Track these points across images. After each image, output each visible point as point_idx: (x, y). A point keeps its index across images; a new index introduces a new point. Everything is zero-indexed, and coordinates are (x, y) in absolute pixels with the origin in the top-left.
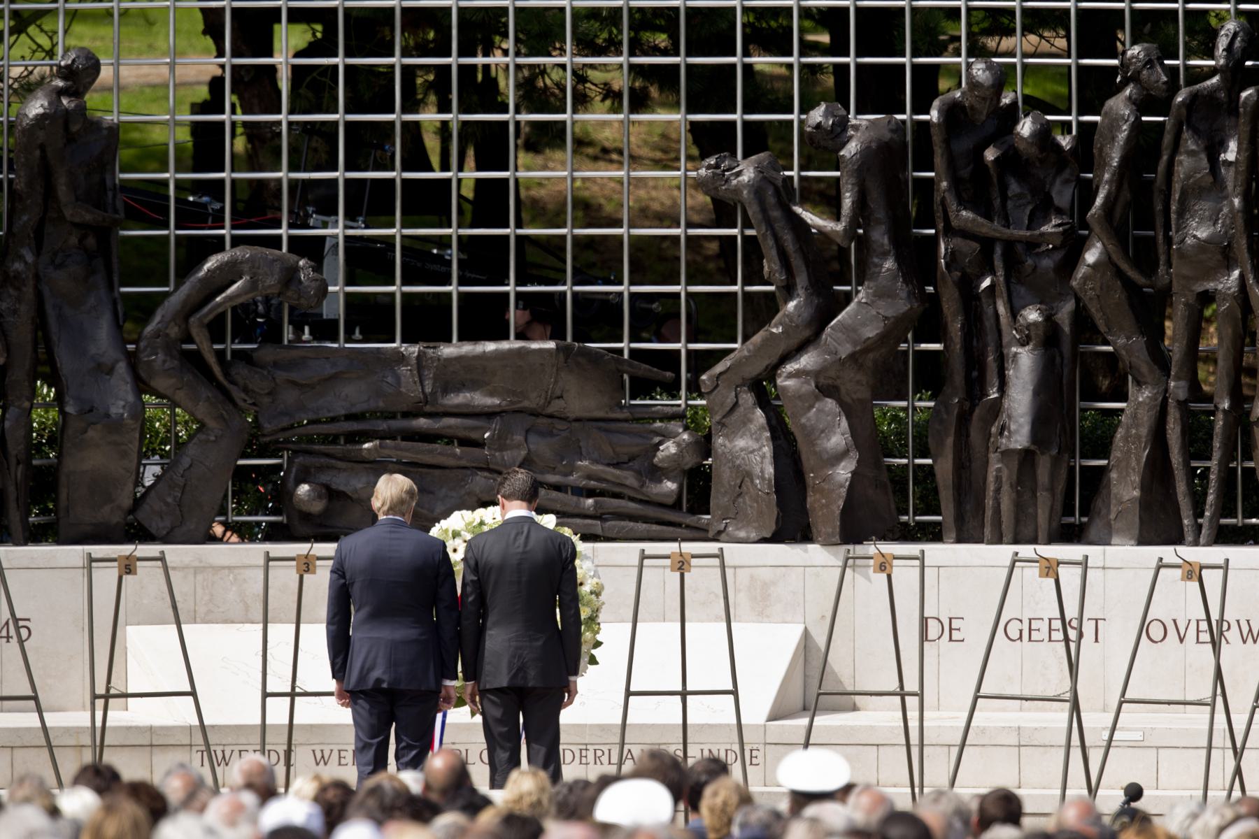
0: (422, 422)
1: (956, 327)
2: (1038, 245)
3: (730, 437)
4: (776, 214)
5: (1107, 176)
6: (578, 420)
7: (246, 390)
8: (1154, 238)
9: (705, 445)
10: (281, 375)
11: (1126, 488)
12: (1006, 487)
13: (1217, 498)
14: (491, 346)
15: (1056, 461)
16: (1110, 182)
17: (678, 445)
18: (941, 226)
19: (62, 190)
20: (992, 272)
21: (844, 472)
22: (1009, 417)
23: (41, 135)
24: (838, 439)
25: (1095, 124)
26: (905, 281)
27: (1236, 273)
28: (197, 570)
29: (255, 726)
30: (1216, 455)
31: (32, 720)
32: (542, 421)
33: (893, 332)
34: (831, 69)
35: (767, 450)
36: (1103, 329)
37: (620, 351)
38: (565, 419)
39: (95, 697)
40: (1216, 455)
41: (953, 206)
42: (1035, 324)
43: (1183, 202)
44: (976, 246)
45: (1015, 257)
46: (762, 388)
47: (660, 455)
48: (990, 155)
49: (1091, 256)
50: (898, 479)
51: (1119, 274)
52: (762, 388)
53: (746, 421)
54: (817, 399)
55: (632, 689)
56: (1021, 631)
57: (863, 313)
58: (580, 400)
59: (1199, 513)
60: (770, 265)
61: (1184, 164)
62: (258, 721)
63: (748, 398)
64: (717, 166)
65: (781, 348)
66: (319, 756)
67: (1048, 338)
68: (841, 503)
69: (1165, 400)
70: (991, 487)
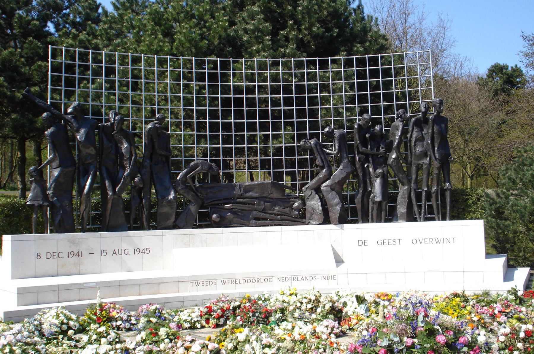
0: (241, 200)
7: (201, 193)
9: (304, 203)
10: (209, 191)
11: (402, 209)
19: (156, 146)
20: (369, 162)
21: (338, 208)
24: (337, 200)
27: (428, 159)
32: (268, 199)
34: (77, 230)
35: (320, 204)
38: (272, 199)
41: (360, 147)
42: (381, 173)
46: (317, 190)
48: (367, 136)
52: (317, 190)
56: (382, 243)
57: (338, 173)
59: (420, 214)
60: (318, 162)
61: (415, 135)
63: (314, 192)
65: (322, 180)
67: (384, 177)
70: (370, 210)
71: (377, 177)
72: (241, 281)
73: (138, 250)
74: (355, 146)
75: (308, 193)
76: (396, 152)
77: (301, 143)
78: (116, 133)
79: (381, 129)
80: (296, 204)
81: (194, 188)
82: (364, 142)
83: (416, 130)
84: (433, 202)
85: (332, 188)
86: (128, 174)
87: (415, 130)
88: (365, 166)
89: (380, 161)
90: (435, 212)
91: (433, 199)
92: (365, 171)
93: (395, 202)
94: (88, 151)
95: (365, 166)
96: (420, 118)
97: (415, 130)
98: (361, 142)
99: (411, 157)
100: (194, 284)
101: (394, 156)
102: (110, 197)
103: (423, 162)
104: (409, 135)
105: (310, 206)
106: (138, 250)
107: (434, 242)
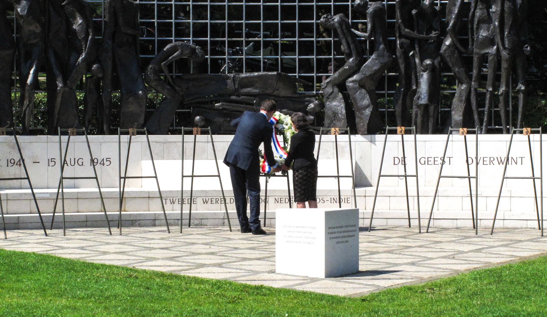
2: (428, 41)
4: (345, 31)
5: (454, 17)
6: (283, 97)
8: (468, 39)
9: (322, 105)
11: (457, 116)
12: (419, 116)
13: (487, 119)
14: (256, 74)
15: (435, 108)
16: (455, 18)
17: (314, 104)
18: (397, 35)
19: (121, 20)
20: (414, 49)
21: (368, 112)
22: (421, 94)
24: (366, 101)
25: (446, 3)
26: (387, 52)
27: (495, 47)
28: (164, 143)
29: (188, 191)
31: (30, 191)
33: (383, 67)
35: (343, 105)
36: (451, 65)
37: (296, 76)
39: (121, 178)
41: (403, 27)
42: (429, 64)
43: (478, 24)
44: (408, 41)
45: (423, 43)
46: (342, 87)
47: (308, 108)
48: (414, 12)
49: (448, 43)
50: (382, 114)
51: (457, 48)
52: (342, 87)
54: (359, 89)
55: (382, 174)
57: (372, 63)
60: (343, 48)
61: (478, 13)
62: (180, 189)
63: (336, 90)
64: (326, 17)
66: (205, 201)
67: (433, 71)
68: (367, 121)
69: (470, 88)
71: (424, 71)
73: (12, 161)
74: (397, 26)
75: (329, 90)
76: (451, 37)
77: (322, 19)
78: (66, 4)
80: (312, 105)
81: (170, 80)
83: (481, 6)
84: (501, 108)
85: (361, 84)
86: (83, 60)
87: (480, 6)
88: (411, 54)
89: (431, 49)
90: (503, 122)
91: (501, 105)
92: (409, 62)
93: (450, 106)
94: (32, 28)
95: (411, 54)
97: (480, 6)
98: (403, 22)
99: (473, 45)
100: (168, 201)
101: (448, 43)
102: (60, 90)
103: (487, 51)
104: (470, 14)
105: (331, 108)
106: (12, 161)
107: (496, 162)
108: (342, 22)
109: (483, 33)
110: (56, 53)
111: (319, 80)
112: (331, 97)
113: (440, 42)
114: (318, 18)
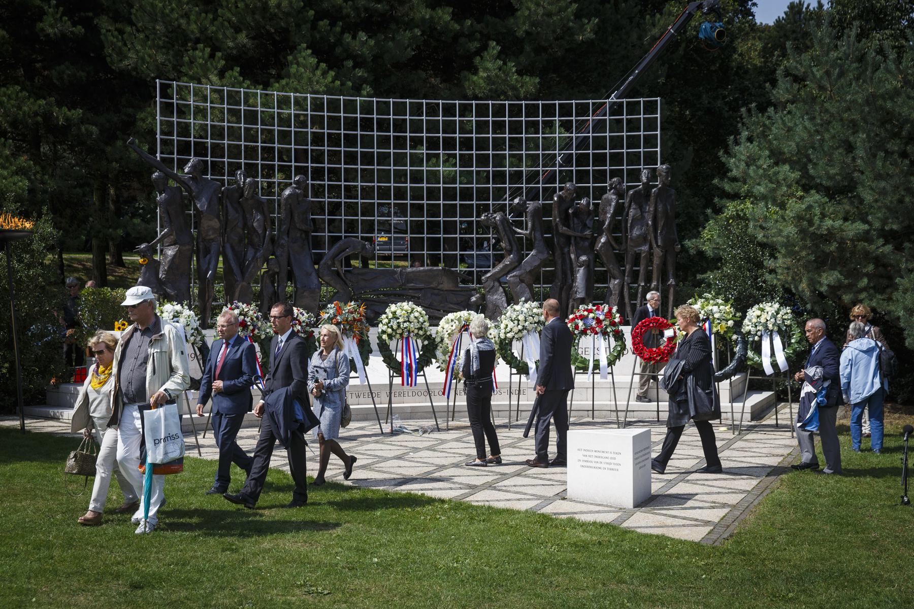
1: (559, 262)
3: (493, 295)
19: (296, 218)
23: (290, 201)
30: (639, 299)
32: (436, 291)
40: (639, 299)
49: (603, 240)
51: (611, 245)
53: (497, 290)
57: (532, 256)
58: (446, 285)
61: (632, 212)
63: (497, 284)
65: (509, 268)
71: (580, 267)
72: (410, 394)
79: (588, 203)
80: (473, 299)
82: (566, 219)
87: (633, 206)
96: (640, 190)
97: (633, 206)
100: (354, 396)
101: (603, 240)
108: (504, 220)
109: (636, 232)
110: (232, 248)
111: (480, 274)
112: (492, 290)
113: (594, 241)
114: (478, 216)
